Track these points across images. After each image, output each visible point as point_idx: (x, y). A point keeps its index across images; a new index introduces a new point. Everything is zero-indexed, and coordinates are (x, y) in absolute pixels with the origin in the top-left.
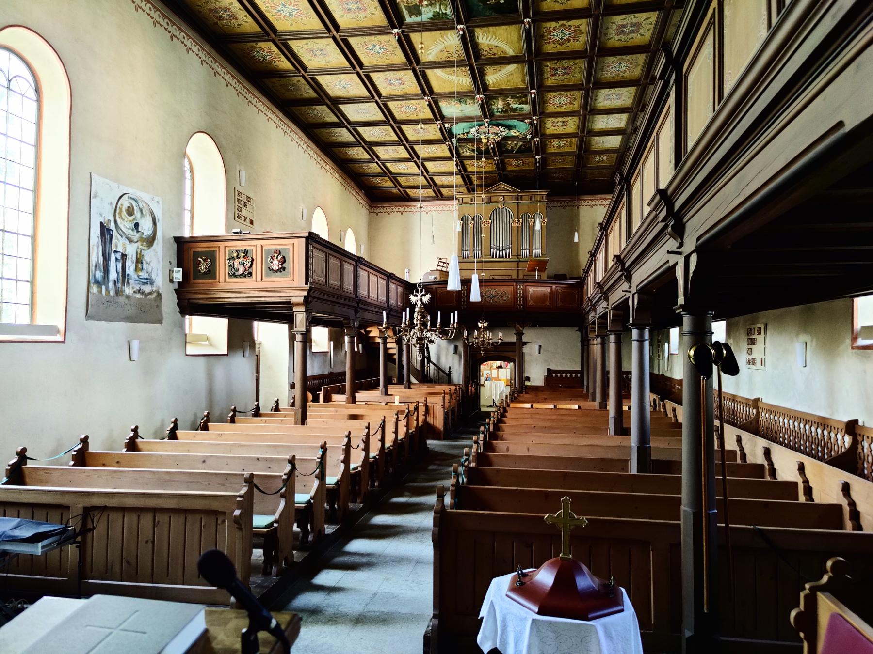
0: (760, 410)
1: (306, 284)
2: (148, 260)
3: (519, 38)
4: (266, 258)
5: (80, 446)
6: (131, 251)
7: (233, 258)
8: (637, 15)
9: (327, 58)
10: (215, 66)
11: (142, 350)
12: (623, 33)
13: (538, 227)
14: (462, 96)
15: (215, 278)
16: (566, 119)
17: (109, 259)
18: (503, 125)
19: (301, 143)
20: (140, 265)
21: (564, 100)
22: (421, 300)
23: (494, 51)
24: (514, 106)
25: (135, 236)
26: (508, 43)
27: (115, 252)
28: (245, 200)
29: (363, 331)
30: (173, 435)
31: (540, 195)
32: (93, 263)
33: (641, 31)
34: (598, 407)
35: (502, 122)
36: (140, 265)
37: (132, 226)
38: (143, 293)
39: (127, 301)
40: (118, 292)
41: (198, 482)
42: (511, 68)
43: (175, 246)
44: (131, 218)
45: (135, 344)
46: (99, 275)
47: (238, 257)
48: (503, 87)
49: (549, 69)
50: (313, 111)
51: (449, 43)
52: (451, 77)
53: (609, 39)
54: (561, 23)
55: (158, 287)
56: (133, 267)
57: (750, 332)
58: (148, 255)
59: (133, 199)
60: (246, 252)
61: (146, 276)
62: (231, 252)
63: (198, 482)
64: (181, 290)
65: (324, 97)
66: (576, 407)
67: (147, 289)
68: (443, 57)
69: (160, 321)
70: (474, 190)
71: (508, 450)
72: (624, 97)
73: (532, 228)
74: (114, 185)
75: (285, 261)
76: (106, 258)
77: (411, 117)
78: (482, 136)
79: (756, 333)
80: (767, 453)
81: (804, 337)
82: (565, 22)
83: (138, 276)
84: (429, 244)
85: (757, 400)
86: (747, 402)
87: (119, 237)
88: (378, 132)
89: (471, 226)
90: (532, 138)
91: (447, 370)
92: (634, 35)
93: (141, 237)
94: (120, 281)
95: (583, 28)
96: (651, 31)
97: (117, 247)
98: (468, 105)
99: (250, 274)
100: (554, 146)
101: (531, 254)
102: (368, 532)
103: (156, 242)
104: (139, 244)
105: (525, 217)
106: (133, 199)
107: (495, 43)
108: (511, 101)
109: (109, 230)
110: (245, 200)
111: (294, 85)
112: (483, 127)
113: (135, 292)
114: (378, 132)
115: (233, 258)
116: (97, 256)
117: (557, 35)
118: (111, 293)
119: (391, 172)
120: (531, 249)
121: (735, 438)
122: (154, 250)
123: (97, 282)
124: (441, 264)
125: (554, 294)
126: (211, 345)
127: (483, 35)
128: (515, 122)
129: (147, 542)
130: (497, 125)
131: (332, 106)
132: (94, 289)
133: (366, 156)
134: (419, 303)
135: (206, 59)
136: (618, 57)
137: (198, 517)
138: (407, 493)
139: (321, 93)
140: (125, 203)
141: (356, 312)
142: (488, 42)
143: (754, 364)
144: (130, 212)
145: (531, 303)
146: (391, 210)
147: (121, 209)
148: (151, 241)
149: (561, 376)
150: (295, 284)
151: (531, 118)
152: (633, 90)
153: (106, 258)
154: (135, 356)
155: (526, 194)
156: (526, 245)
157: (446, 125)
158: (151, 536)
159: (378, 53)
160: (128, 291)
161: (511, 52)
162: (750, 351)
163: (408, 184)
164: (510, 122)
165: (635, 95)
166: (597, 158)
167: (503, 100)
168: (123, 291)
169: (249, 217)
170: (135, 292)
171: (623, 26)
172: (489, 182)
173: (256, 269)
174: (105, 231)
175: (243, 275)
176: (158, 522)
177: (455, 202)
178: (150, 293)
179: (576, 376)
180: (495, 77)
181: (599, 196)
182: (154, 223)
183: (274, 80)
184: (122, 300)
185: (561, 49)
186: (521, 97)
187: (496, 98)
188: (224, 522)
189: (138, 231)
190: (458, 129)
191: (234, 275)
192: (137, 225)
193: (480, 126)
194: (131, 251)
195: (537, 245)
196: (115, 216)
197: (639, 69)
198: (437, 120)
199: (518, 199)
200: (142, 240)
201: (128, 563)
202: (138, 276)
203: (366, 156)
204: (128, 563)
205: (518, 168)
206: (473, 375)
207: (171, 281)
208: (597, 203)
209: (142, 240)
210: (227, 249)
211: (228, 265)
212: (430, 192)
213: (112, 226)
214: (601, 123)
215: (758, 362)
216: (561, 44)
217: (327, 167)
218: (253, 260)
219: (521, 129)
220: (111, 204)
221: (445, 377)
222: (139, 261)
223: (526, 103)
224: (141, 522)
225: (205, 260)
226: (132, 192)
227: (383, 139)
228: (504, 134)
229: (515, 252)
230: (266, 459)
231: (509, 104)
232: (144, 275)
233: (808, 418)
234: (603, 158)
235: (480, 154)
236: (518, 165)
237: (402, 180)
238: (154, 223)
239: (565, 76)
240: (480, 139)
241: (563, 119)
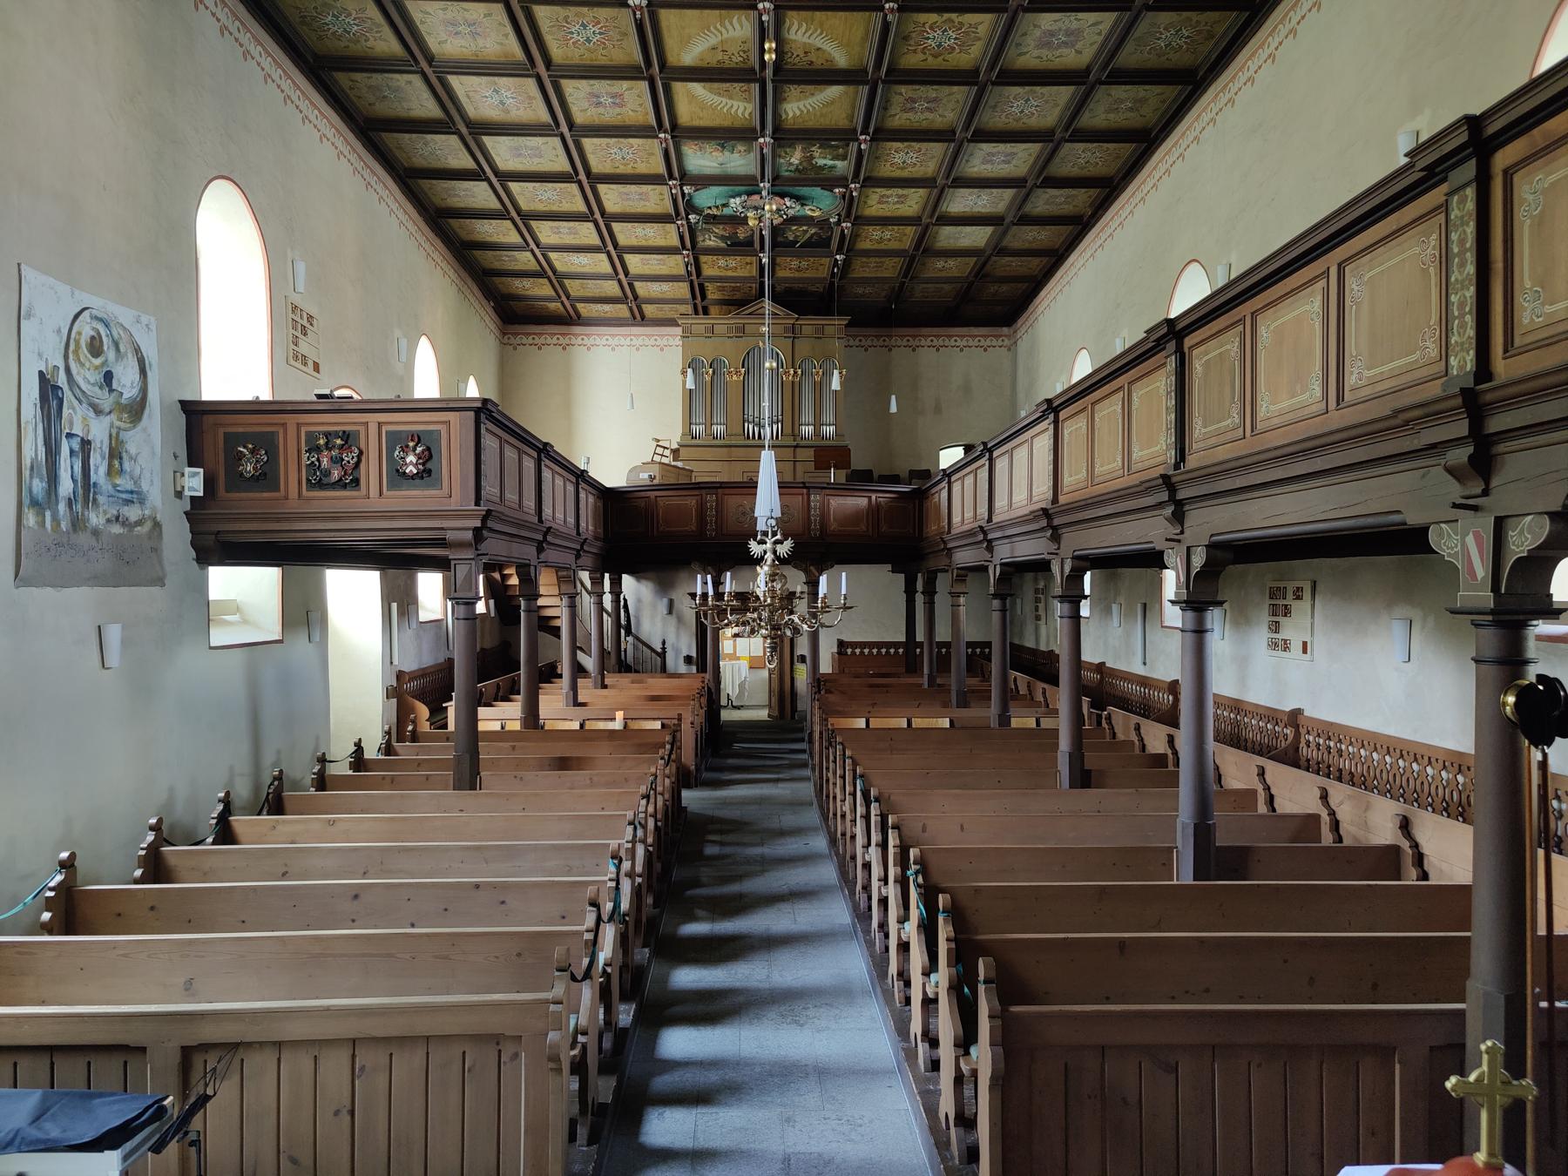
0: (1303, 731)
1: (477, 504)
2: (133, 451)
3: (865, 39)
4: (391, 451)
5: (59, 878)
6: (99, 431)
7: (318, 449)
8: (1080, 15)
9: (481, 42)
10: (245, 38)
11: (125, 642)
12: (1048, 45)
13: (836, 384)
14: (725, 136)
15: (278, 490)
16: (905, 191)
17: (58, 452)
18: (792, 196)
19: (395, 206)
20: (116, 463)
21: (912, 158)
22: (775, 552)
23: (812, 57)
24: (821, 162)
25: (106, 401)
26: (841, 45)
27: (69, 436)
28: (305, 322)
29: (497, 576)
30: (225, 833)
31: (836, 324)
32: (27, 462)
33: (1079, 46)
34: (994, 723)
35: (791, 189)
36: (116, 463)
37: (99, 377)
38: (125, 523)
39: (94, 543)
40: (77, 523)
41: (390, 955)
42: (834, 91)
43: (182, 419)
44: (97, 362)
45: (114, 634)
46: (39, 486)
47: (328, 447)
48: (811, 124)
49: (901, 99)
50: (426, 144)
51: (732, 33)
52: (717, 99)
53: (1020, 55)
54: (946, 16)
55: (154, 509)
56: (103, 469)
57: (1275, 593)
58: (134, 441)
59: (101, 320)
60: (346, 436)
61: (130, 486)
62: (311, 437)
63: (390, 955)
64: (197, 511)
65: (457, 118)
66: (945, 723)
67: (133, 513)
68: (713, 60)
69: (159, 581)
70: (706, 312)
71: (924, 830)
72: (1018, 159)
73: (820, 388)
74: (64, 289)
75: (431, 457)
76: (52, 451)
77: (622, 170)
78: (750, 214)
79: (1290, 595)
80: (1405, 825)
81: (1403, 610)
82: (954, 16)
83: (115, 486)
84: (623, 410)
85: (1296, 713)
86: (1271, 715)
87: (76, 403)
88: (549, 194)
89: (708, 378)
90: (838, 223)
91: (659, 649)
92: (1065, 51)
93: (118, 403)
94: (80, 499)
95: (983, 30)
96: (1096, 47)
97: (71, 424)
98: (736, 155)
99: (356, 482)
100: (873, 237)
101: (817, 433)
102: (678, 1009)
103: (147, 412)
104: (113, 417)
105: (807, 365)
106: (101, 320)
107: (818, 42)
108: (816, 151)
109: (56, 388)
110: (305, 322)
111: (397, 90)
112: (756, 197)
113: (108, 521)
114: (549, 194)
115: (318, 449)
116: (33, 448)
117: (934, 39)
118: (64, 526)
119: (554, 271)
120: (818, 424)
121: (1318, 793)
122: (145, 430)
123: (35, 503)
124: (660, 450)
125: (874, 510)
126: (245, 622)
127: (800, 26)
128: (817, 192)
129: (337, 1113)
130: (782, 196)
131: (469, 139)
132: (30, 519)
133: (514, 238)
134: (769, 557)
135: (228, 23)
136: (1027, 88)
137: (456, 1051)
138: (700, 913)
139: (449, 105)
140: (86, 329)
141: (540, 550)
142: (805, 40)
143: (1286, 648)
144: (95, 348)
145: (833, 526)
146: (542, 340)
147: (77, 342)
148: (136, 410)
149: (862, 653)
150: (454, 504)
151: (846, 187)
152: (1035, 148)
153: (52, 451)
154: (113, 658)
155: (808, 324)
156: (807, 415)
157: (687, 189)
158: (347, 1102)
159: (588, 40)
160: (95, 519)
161: (841, 60)
162: (1275, 627)
163: (582, 293)
164: (805, 191)
165: (1038, 157)
166: (940, 264)
167: (804, 150)
168: (86, 520)
169: (312, 356)
170: (108, 521)
171: (1052, 34)
172: (740, 301)
173: (372, 472)
174: (49, 391)
175: (340, 484)
176: (362, 1068)
177: (679, 330)
178: (139, 523)
179: (896, 652)
180: (800, 106)
181: (925, 331)
182: (143, 372)
183: (358, 76)
184: (84, 539)
185: (933, 63)
186: (837, 147)
187: (792, 146)
188: (516, 1056)
189: (111, 390)
190: (707, 198)
191: (320, 485)
192: (108, 377)
193: (749, 194)
194: (99, 431)
195: (829, 416)
196: (66, 357)
197: (1056, 112)
198: (671, 177)
199: (793, 333)
200: (120, 408)
201: (294, 1161)
202: (115, 486)
203: (514, 238)
204: (294, 1161)
205: (797, 275)
206: (705, 658)
207: (179, 495)
208: (923, 342)
209: (120, 408)
210: (303, 430)
211: (305, 461)
212: (622, 310)
213: (62, 380)
214: (962, 202)
215: (1296, 646)
216: (935, 56)
217: (436, 256)
218: (361, 453)
219: (822, 204)
220: (59, 331)
221: (658, 661)
222: (115, 453)
223: (844, 158)
224: (321, 1070)
225: (252, 452)
226: (97, 303)
227: (555, 208)
228: (791, 212)
229: (788, 430)
230: (494, 886)
231: (812, 157)
232: (124, 483)
233: (1420, 752)
234: (951, 263)
235: (740, 247)
236: (799, 269)
237: (574, 287)
238: (143, 372)
239: (928, 115)
240: (746, 218)
241: (900, 191)
